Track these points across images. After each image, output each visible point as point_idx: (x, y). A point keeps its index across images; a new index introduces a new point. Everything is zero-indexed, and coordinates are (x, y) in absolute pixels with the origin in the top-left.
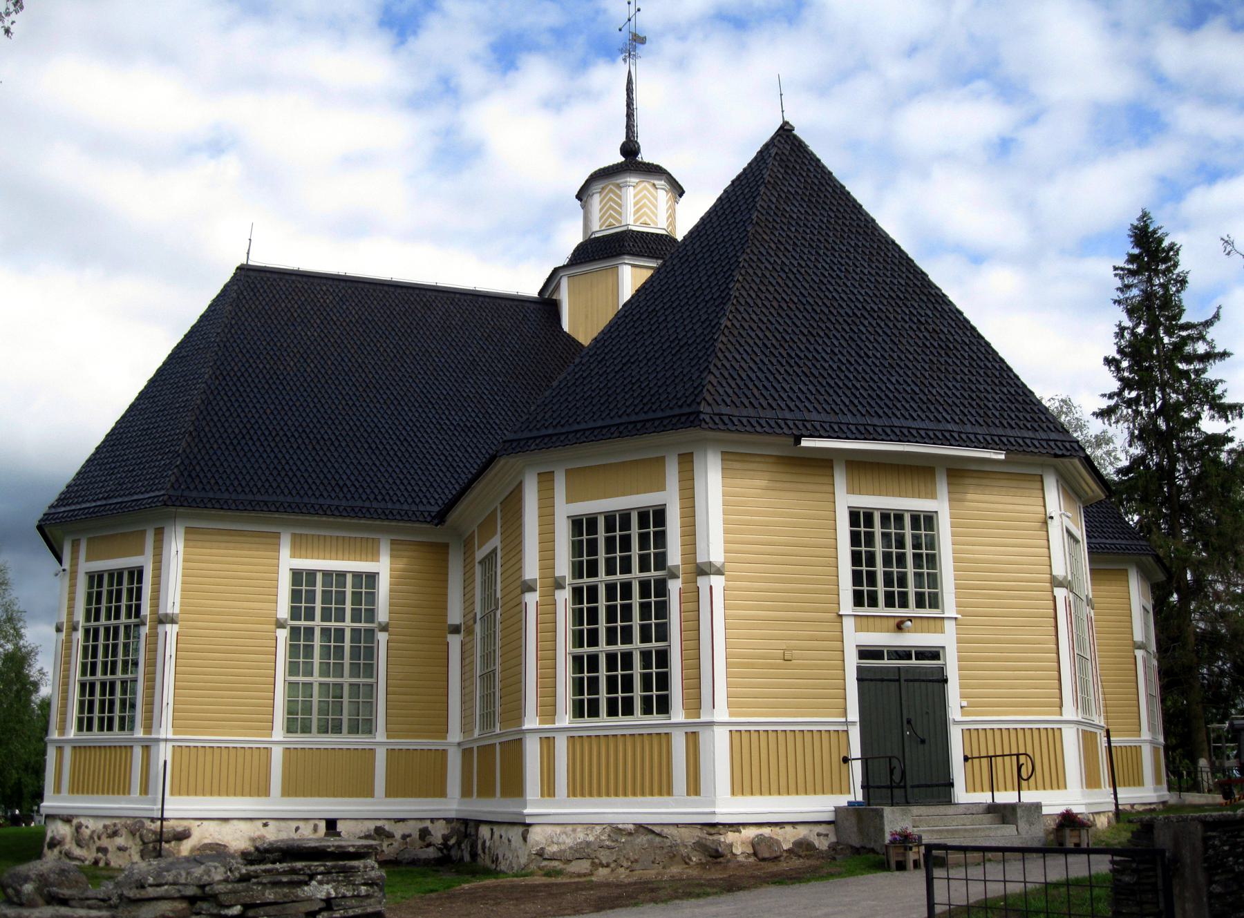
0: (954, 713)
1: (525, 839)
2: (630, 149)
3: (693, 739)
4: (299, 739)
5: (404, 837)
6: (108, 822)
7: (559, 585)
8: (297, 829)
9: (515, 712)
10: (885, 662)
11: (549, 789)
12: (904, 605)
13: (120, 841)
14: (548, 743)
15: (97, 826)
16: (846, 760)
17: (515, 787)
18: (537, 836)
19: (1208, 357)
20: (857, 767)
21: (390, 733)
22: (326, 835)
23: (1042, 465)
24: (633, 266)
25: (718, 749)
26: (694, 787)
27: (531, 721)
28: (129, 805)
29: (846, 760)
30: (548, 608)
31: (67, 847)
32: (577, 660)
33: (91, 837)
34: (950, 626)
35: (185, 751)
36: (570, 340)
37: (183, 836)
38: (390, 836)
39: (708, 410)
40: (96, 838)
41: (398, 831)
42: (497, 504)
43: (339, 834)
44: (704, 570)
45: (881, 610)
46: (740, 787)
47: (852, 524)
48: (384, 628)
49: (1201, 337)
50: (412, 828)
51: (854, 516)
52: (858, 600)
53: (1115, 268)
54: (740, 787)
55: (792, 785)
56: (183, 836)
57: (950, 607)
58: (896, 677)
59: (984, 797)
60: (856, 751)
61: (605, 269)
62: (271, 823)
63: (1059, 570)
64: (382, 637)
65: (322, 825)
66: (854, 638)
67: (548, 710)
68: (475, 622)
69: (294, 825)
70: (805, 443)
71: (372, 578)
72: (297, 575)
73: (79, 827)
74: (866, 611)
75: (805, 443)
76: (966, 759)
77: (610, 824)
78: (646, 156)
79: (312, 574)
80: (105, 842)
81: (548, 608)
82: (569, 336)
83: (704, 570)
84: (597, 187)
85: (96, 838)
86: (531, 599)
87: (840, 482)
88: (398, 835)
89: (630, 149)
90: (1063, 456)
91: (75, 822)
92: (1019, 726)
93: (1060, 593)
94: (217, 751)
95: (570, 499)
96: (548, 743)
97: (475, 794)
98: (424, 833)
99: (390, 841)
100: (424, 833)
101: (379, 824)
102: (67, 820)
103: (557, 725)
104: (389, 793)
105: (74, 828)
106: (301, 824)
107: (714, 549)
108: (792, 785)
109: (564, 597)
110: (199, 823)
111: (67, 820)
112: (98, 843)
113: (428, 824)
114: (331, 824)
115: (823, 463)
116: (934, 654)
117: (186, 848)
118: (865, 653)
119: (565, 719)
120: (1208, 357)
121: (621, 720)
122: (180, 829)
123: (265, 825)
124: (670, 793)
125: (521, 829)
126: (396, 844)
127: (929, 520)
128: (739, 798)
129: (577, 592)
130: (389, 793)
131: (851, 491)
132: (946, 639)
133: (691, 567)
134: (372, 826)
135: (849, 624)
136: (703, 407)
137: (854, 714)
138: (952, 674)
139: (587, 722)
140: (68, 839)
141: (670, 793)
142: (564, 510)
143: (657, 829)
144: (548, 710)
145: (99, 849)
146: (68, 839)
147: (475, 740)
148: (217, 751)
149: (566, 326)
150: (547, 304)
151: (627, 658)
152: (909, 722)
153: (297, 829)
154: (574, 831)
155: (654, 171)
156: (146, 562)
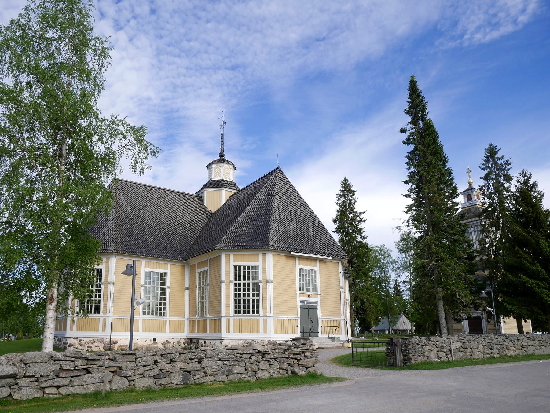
0: (319, 316)
1: (221, 343)
2: (221, 156)
3: (265, 320)
4: (147, 317)
5: (174, 343)
6: (91, 339)
7: (231, 282)
8: (146, 341)
9: (219, 312)
10: (311, 304)
11: (228, 331)
12: (309, 291)
13: (95, 344)
14: (228, 321)
15: (88, 340)
16: (297, 326)
17: (219, 330)
18: (225, 342)
19: (359, 222)
20: (299, 328)
21: (170, 316)
22: (154, 343)
23: (339, 260)
24: (225, 190)
25: (271, 323)
26: (265, 331)
27: (223, 314)
28: (99, 334)
29: (297, 326)
30: (228, 288)
31: (76, 346)
32: (236, 301)
33: (85, 343)
34: (319, 296)
35: (116, 319)
36: (205, 210)
37: (115, 343)
38: (170, 343)
39: (271, 244)
40: (87, 344)
41: (172, 341)
42: (208, 259)
43: (157, 343)
44: (267, 281)
45: (305, 292)
46: (276, 332)
47: (299, 272)
48: (169, 288)
49: (359, 216)
50: (176, 341)
51: (300, 270)
52: (300, 290)
53: (337, 194)
54: (276, 332)
55: (277, 332)
56: (115, 343)
57: (319, 292)
58: (307, 308)
59: (327, 336)
60: (299, 324)
61: (220, 190)
62: (139, 339)
63: (341, 285)
64: (168, 290)
65: (153, 340)
66: (300, 298)
67: (228, 312)
68: (196, 288)
69: (145, 340)
70: (292, 253)
71: (315, 271)
72: (146, 272)
73: (80, 341)
74: (302, 292)
75: (292, 253)
76: (322, 327)
77: (245, 340)
78: (226, 158)
79: (150, 273)
80: (90, 345)
81: (228, 288)
82: (206, 208)
83: (267, 281)
84: (214, 165)
85: (87, 344)
86: (224, 285)
87: (297, 261)
88: (172, 343)
89: (221, 156)
90: (344, 259)
91: (79, 339)
92: (332, 320)
93: (341, 290)
94: (125, 320)
95: (234, 262)
96: (228, 321)
97: (445, 330)
98: (179, 342)
99: (170, 344)
100: (179, 342)
101: (167, 340)
102: (76, 338)
103: (231, 316)
104: (170, 331)
105: (78, 341)
106: (147, 339)
107: (270, 276)
108: (277, 332)
109: (232, 285)
110: (120, 339)
111: (76, 338)
112: (88, 345)
113: (179, 340)
114: (155, 340)
115: (294, 257)
116: (315, 303)
117: (117, 345)
118: (301, 302)
119: (232, 313)
120: (359, 222)
121: (247, 315)
122: (115, 341)
123: (138, 340)
124: (165, 332)
125: (219, 341)
126: (171, 345)
127: (315, 271)
128: (275, 334)
129: (236, 284)
130: (170, 331)
131: (299, 264)
132: (318, 299)
133: (265, 280)
134: (165, 340)
135: (298, 295)
136: (270, 243)
137: (299, 316)
138: (319, 307)
139: (238, 315)
140: (77, 344)
141: (165, 332)
142: (233, 264)
143: (256, 341)
144: (228, 312)
145: (88, 347)
146: (77, 344)
147: (197, 318)
148: (125, 320)
149: (205, 204)
150: (199, 197)
151: (249, 301)
152: (310, 318)
153: (146, 341)
154: (235, 341)
155: (229, 163)
156: (260, 263)
